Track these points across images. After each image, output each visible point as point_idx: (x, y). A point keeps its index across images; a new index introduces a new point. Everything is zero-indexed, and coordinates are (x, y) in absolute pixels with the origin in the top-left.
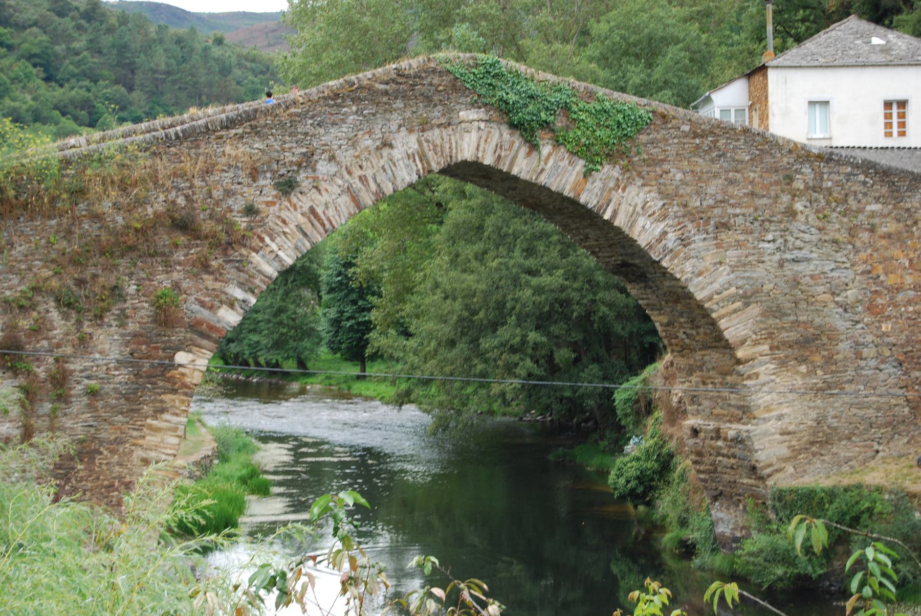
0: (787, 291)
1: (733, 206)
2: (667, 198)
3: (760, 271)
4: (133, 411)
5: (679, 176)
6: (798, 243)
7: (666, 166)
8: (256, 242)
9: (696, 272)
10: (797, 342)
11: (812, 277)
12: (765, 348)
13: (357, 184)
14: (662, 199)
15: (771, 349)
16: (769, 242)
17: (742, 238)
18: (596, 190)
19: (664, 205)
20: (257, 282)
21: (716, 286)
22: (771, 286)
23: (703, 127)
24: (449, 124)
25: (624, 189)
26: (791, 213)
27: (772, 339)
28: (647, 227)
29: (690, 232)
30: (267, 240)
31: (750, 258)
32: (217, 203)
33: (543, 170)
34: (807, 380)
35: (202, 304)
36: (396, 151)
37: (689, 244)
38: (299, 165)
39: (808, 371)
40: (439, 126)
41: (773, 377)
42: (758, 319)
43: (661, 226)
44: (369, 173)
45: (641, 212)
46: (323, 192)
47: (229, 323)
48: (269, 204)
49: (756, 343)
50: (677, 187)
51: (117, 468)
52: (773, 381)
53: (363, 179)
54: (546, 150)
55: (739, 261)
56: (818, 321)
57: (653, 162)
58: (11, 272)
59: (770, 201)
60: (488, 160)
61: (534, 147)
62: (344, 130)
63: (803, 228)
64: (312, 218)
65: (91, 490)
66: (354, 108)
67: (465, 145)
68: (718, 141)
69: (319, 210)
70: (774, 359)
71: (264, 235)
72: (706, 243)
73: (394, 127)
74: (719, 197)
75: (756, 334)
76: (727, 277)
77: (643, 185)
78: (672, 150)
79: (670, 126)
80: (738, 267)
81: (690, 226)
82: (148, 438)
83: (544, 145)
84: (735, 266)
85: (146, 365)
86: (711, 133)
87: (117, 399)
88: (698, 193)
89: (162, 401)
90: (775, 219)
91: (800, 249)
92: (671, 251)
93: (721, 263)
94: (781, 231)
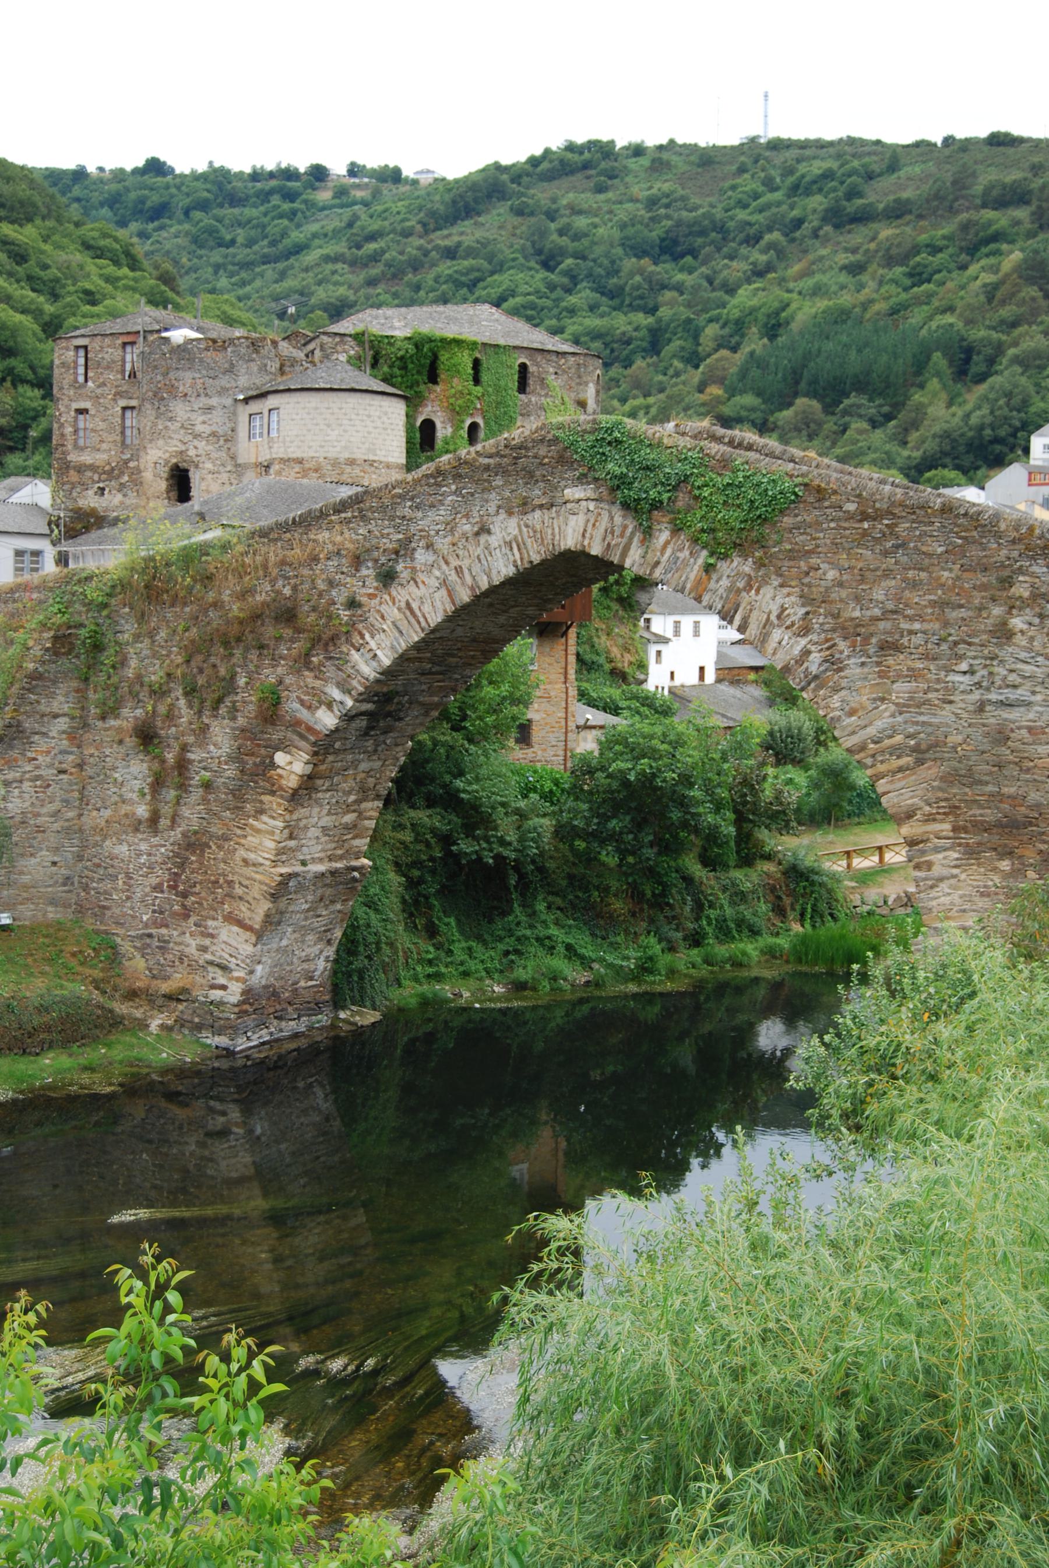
0: (986, 747)
1: (911, 619)
2: (810, 604)
3: (946, 715)
4: (237, 808)
5: (832, 574)
6: (1012, 678)
7: (814, 561)
8: (356, 639)
9: (847, 709)
10: (999, 825)
11: (1030, 729)
12: (946, 827)
13: (453, 577)
14: (803, 605)
15: (955, 829)
16: (965, 673)
17: (919, 665)
18: (721, 591)
19: (807, 613)
20: (355, 683)
21: (871, 731)
22: (959, 739)
23: (878, 505)
24: (552, 505)
25: (758, 591)
26: (1003, 633)
27: (957, 816)
28: (784, 643)
29: (842, 652)
30: (367, 636)
31: (930, 696)
32: (320, 595)
33: (658, 563)
34: (1012, 883)
35: (302, 702)
36: (493, 537)
37: (840, 670)
38: (397, 553)
39: (1013, 870)
40: (541, 507)
41: (955, 871)
42: (935, 784)
43: (803, 642)
44: (465, 564)
45: (776, 622)
46: (421, 585)
47: (325, 726)
48: (372, 596)
49: (930, 819)
50: (827, 589)
51: (222, 865)
52: (954, 876)
53: (459, 570)
54: (663, 536)
55: (911, 698)
56: (1034, 796)
57: (793, 555)
58: (154, 656)
59: (970, 613)
60: (596, 550)
61: (648, 533)
62: (442, 513)
63: (1023, 655)
64: (408, 613)
65: (201, 883)
66: (453, 487)
67: (570, 531)
68: (896, 525)
69: (415, 606)
70: (960, 845)
71: (365, 632)
72: (866, 670)
73: (492, 510)
74: (890, 605)
75: (930, 805)
76: (891, 720)
77: (782, 586)
78: (824, 539)
79: (827, 504)
80: (909, 706)
81: (842, 645)
82: (249, 838)
83: (660, 530)
84: (904, 706)
85: (250, 761)
86: (889, 513)
87: (226, 794)
88: (857, 599)
89: (261, 802)
90: (976, 640)
91: (1015, 687)
92: (816, 677)
93: (883, 700)
94: (986, 658)
